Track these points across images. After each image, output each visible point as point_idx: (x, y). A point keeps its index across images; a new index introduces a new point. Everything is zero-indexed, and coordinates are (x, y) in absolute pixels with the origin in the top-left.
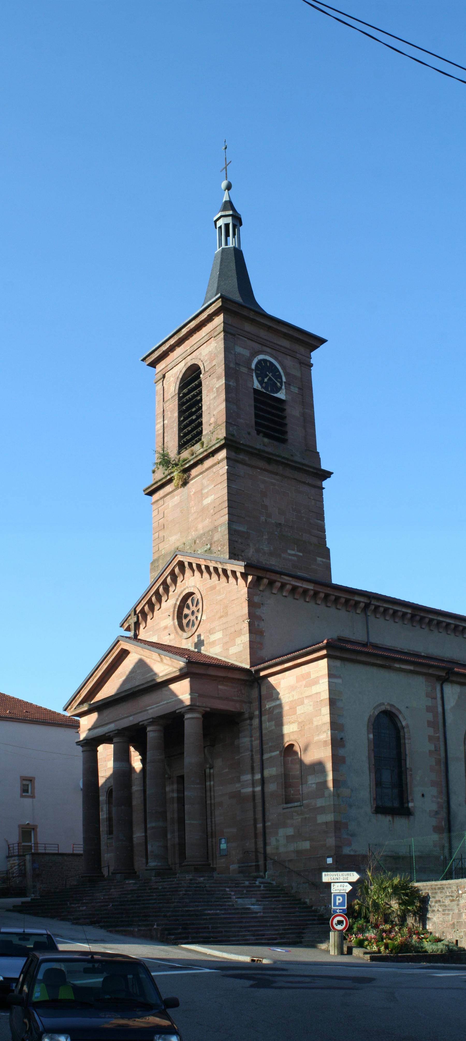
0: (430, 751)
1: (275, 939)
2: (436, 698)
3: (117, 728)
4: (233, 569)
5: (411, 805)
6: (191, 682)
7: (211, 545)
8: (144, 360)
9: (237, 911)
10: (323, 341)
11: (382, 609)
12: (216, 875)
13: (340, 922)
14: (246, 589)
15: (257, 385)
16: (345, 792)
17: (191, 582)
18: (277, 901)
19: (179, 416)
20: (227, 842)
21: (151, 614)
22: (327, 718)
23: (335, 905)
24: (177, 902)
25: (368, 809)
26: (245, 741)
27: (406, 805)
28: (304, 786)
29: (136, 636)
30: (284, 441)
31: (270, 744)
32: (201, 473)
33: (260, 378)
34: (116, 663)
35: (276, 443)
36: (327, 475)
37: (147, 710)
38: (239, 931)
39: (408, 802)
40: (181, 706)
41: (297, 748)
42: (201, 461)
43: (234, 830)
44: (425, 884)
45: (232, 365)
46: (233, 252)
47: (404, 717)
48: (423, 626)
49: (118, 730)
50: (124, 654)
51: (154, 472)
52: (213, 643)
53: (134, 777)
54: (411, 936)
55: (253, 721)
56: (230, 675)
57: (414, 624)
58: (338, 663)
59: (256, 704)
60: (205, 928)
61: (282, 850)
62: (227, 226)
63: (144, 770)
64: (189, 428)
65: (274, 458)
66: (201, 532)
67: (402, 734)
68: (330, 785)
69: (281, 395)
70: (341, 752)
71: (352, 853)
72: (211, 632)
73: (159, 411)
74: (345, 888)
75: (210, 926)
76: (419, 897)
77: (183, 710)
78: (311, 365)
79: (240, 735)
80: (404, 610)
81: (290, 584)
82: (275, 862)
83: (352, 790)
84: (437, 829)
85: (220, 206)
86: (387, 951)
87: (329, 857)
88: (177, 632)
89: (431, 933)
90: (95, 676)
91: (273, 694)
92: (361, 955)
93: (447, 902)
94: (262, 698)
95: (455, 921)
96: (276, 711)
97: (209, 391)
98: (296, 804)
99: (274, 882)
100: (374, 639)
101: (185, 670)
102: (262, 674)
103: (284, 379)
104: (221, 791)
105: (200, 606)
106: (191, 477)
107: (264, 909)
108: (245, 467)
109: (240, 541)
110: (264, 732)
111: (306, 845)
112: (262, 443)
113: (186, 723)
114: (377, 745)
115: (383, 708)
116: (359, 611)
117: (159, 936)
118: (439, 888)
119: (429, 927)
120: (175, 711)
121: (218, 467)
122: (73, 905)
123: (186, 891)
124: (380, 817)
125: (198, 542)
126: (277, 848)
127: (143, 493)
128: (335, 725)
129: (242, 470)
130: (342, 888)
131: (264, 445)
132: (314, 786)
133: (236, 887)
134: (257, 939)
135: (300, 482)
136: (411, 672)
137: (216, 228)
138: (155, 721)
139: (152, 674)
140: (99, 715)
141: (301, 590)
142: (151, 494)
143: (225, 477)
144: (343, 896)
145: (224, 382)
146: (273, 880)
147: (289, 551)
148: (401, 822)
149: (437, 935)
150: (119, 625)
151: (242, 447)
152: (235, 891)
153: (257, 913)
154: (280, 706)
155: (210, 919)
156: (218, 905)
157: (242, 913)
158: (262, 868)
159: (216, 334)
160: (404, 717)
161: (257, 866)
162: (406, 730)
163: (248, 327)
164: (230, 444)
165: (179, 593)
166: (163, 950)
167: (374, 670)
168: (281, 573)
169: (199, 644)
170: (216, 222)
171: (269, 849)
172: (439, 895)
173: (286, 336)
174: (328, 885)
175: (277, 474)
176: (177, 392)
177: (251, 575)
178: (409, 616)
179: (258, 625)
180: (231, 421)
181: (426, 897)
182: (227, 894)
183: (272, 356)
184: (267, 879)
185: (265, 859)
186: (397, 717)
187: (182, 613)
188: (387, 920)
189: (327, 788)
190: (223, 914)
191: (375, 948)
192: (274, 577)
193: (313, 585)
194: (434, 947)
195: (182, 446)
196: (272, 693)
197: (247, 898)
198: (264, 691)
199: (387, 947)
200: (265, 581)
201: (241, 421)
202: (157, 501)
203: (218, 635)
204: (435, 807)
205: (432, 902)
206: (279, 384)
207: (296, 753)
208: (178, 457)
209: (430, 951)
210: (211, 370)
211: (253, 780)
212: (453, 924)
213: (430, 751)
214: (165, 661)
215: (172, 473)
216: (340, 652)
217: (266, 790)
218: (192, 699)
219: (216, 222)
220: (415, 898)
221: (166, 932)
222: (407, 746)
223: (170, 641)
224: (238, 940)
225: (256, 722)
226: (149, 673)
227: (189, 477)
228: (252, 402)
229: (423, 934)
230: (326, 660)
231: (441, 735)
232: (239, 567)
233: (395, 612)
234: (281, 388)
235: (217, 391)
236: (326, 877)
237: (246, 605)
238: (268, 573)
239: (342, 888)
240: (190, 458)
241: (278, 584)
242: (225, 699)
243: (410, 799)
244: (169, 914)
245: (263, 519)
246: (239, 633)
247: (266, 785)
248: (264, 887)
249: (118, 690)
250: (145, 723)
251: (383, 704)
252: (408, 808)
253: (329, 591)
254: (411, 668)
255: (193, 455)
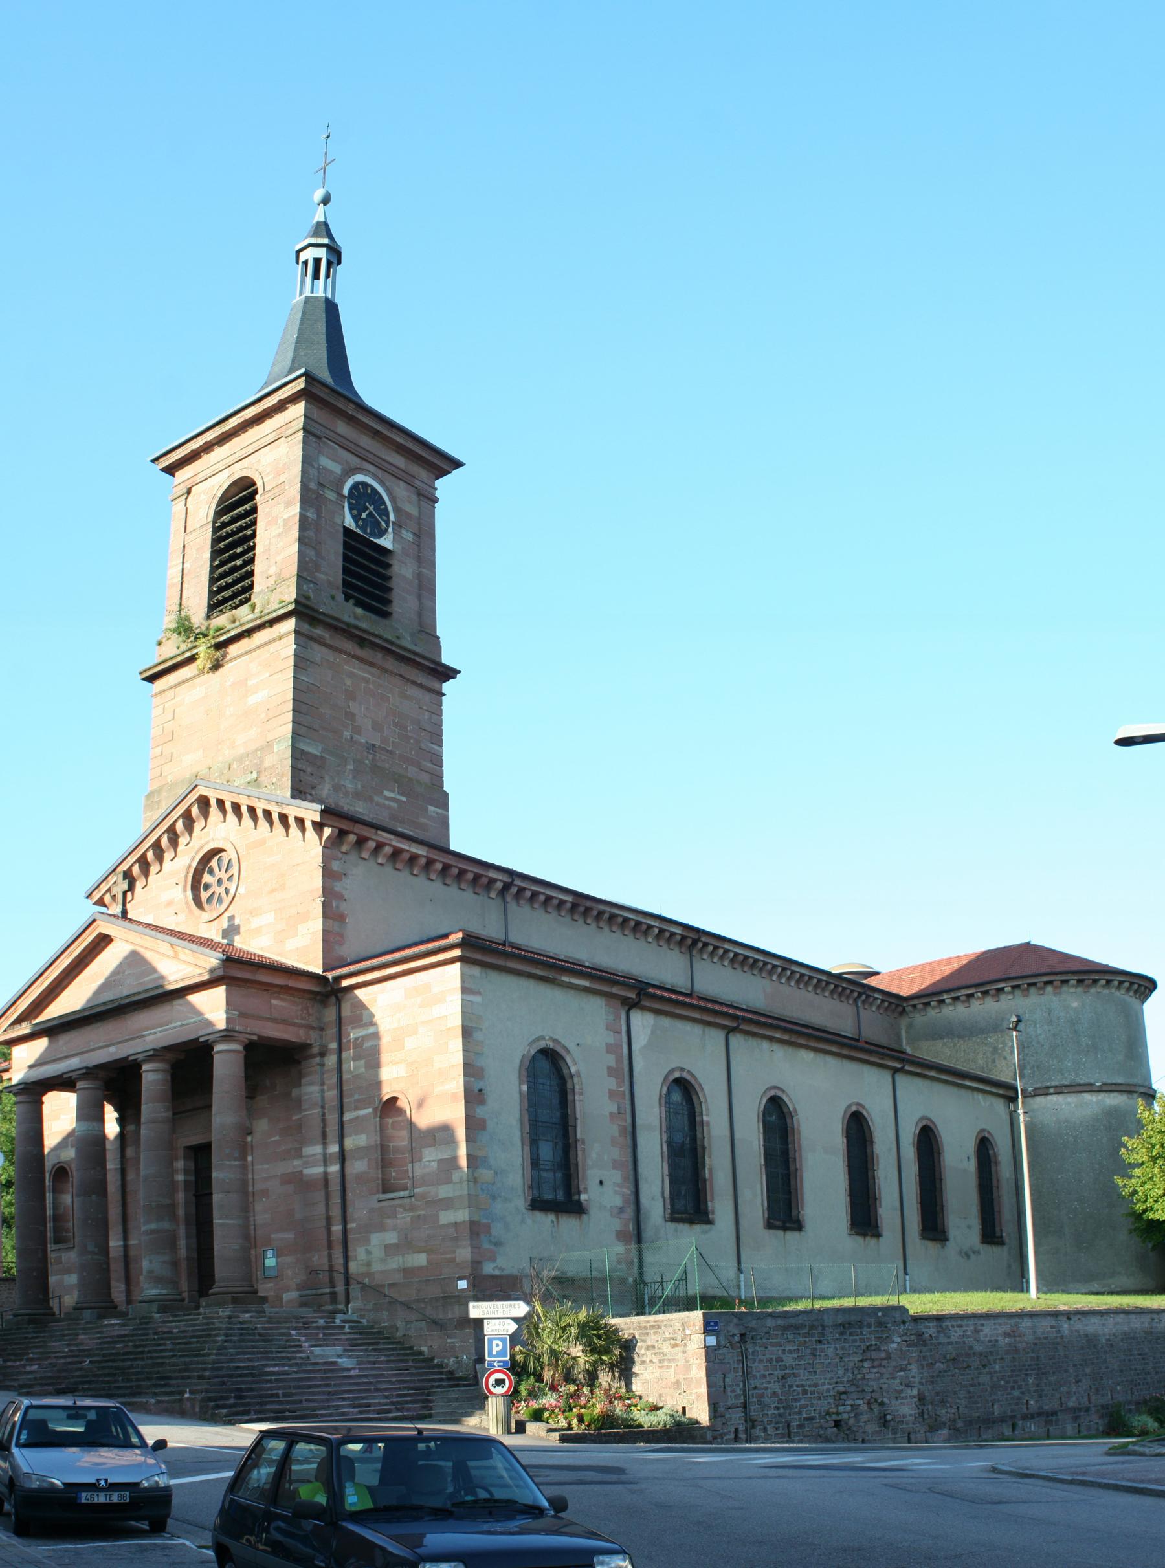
0: (611, 1114)
1: (389, 1411)
2: (619, 1033)
3: (84, 1065)
4: (300, 815)
5: (583, 1197)
6: (227, 991)
7: (259, 773)
8: (155, 460)
9: (317, 1368)
10: (457, 464)
11: (528, 894)
12: (267, 1308)
13: (499, 1382)
14: (320, 849)
15: (349, 522)
16: (485, 1174)
17: (217, 831)
18: (375, 1350)
19: (213, 559)
20: (277, 1255)
21: (143, 879)
22: (458, 1058)
23: (490, 1355)
24: (217, 1354)
25: (520, 1202)
26: (311, 1090)
27: (575, 1198)
28: (417, 1165)
29: (124, 913)
30: (386, 615)
31: (356, 1097)
32: (248, 652)
33: (355, 512)
34: (86, 957)
35: (373, 617)
36: (450, 673)
37: (144, 1036)
38: (328, 1400)
39: (579, 1193)
40: (209, 1031)
41: (402, 1103)
42: (249, 633)
43: (290, 1236)
44: (627, 1319)
45: (313, 486)
46: (323, 306)
47: (574, 1060)
48: (589, 921)
49: (87, 1068)
50: (104, 941)
51: (159, 644)
52: (258, 931)
53: (108, 1146)
54: (611, 1402)
55: (326, 1059)
56: (292, 983)
57: (576, 917)
58: (476, 971)
59: (332, 1031)
60: (272, 1395)
61: (376, 1267)
62: (317, 261)
63: (122, 1136)
64: (229, 580)
65: (371, 638)
66: (242, 750)
67: (569, 1085)
68: (463, 1162)
69: (386, 542)
70: (480, 1112)
71: (497, 1272)
72: (253, 913)
73: (175, 544)
74: (506, 1327)
75: (280, 1392)
76: (619, 1341)
77: (212, 1037)
78: (436, 500)
79: (303, 1081)
80: (562, 897)
81: (390, 845)
82: (364, 1287)
83: (496, 1173)
84: (621, 1236)
85: (309, 227)
86: (583, 1426)
87: (460, 1278)
88: (191, 911)
89: (640, 1397)
90: (47, 978)
91: (362, 1015)
92: (543, 1433)
93: (666, 1348)
94: (343, 1021)
95: (681, 1377)
96: (367, 1044)
97: (269, 523)
98: (402, 1194)
99: (364, 1320)
100: (515, 937)
101: (220, 973)
102: (345, 983)
103: (392, 518)
104: (266, 1172)
105: (234, 870)
106: (229, 657)
107: (359, 1363)
108: (323, 649)
109: (309, 770)
110: (345, 1077)
111: (421, 1260)
112: (352, 614)
113: (217, 1059)
114: (533, 1102)
115: (542, 1044)
116: (493, 895)
117: (197, 1410)
118: (652, 1327)
119: (637, 1386)
120: (198, 1039)
121: (279, 648)
122: (9, 1364)
123: (226, 1335)
124: (539, 1216)
125: (234, 766)
126: (368, 1264)
127: (139, 677)
128: (471, 1069)
129: (318, 653)
130: (501, 1327)
131: (356, 618)
132: (434, 1165)
133: (306, 1328)
134: (360, 1412)
135: (408, 680)
136: (586, 990)
137: (297, 262)
138: (156, 1054)
139: (155, 976)
140: (50, 1042)
141: (406, 856)
142: (151, 679)
143: (291, 662)
144: (503, 1340)
145: (298, 510)
146: (362, 1316)
147: (386, 793)
148: (568, 1223)
149: (651, 1400)
150: (84, 895)
151: (321, 617)
152: (305, 1335)
153: (349, 1370)
154: (376, 1036)
155: (276, 1380)
156: (283, 1358)
157: (325, 1371)
158: (341, 1297)
159: (289, 432)
160: (574, 1060)
161: (334, 1295)
162: (576, 1080)
163: (342, 428)
164: (303, 611)
165: (197, 848)
166: (217, 1434)
167: (531, 984)
168: (377, 827)
169: (232, 931)
170: (298, 252)
171: (353, 1267)
172: (653, 1337)
173: (401, 449)
174: (479, 1322)
175: (372, 665)
176: (211, 518)
177: (328, 826)
178: (569, 905)
179: (338, 907)
180: (305, 574)
181: (631, 1340)
182: (294, 1340)
183: (375, 477)
184: (350, 1315)
185: (347, 1283)
186: (563, 1059)
187: (200, 882)
188: (569, 1378)
189: (458, 1168)
190: (296, 1372)
191: (563, 1423)
192: (366, 832)
193: (426, 849)
194: (652, 1418)
195: (215, 606)
196: (362, 1015)
197: (327, 1346)
198: (346, 1011)
199: (581, 1419)
200: (352, 838)
201: (322, 576)
202: (164, 691)
203: (268, 918)
204: (618, 1201)
205: (641, 1348)
206: (383, 524)
207: (401, 1111)
208: (206, 624)
209: (646, 1426)
210: (276, 490)
211: (325, 1155)
212: (678, 1382)
213: (611, 1114)
214: (182, 956)
215: (196, 647)
216: (479, 953)
217: (348, 1171)
218: (228, 1020)
219: (298, 252)
220: (613, 1342)
221: (212, 1404)
222: (578, 1104)
223: (177, 924)
224: (331, 1415)
225: (331, 1060)
226: (150, 974)
227: (224, 656)
228: (341, 549)
229: (629, 1399)
230: (458, 965)
231: (625, 1088)
232: (311, 812)
233: (548, 899)
234: (386, 531)
235: (285, 525)
236: (476, 1310)
237: (319, 873)
238: (358, 825)
239: (501, 1327)
240: (229, 627)
241: (372, 845)
242: (281, 1021)
243: (581, 1187)
244: (207, 1373)
245: (347, 734)
246: (304, 917)
247: (347, 1163)
248: (350, 1328)
249: (88, 1001)
250: (140, 1057)
251: (543, 1038)
252: (579, 1202)
253: (449, 860)
254: (586, 983)
255: (234, 622)
